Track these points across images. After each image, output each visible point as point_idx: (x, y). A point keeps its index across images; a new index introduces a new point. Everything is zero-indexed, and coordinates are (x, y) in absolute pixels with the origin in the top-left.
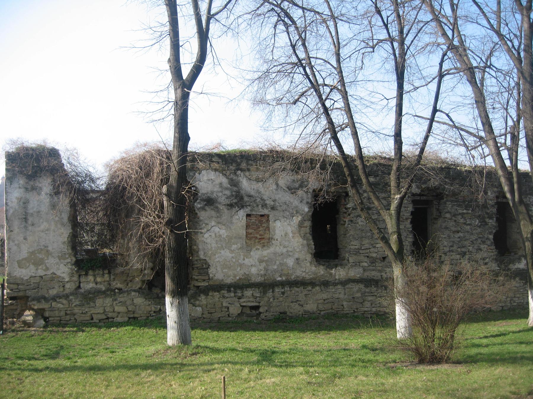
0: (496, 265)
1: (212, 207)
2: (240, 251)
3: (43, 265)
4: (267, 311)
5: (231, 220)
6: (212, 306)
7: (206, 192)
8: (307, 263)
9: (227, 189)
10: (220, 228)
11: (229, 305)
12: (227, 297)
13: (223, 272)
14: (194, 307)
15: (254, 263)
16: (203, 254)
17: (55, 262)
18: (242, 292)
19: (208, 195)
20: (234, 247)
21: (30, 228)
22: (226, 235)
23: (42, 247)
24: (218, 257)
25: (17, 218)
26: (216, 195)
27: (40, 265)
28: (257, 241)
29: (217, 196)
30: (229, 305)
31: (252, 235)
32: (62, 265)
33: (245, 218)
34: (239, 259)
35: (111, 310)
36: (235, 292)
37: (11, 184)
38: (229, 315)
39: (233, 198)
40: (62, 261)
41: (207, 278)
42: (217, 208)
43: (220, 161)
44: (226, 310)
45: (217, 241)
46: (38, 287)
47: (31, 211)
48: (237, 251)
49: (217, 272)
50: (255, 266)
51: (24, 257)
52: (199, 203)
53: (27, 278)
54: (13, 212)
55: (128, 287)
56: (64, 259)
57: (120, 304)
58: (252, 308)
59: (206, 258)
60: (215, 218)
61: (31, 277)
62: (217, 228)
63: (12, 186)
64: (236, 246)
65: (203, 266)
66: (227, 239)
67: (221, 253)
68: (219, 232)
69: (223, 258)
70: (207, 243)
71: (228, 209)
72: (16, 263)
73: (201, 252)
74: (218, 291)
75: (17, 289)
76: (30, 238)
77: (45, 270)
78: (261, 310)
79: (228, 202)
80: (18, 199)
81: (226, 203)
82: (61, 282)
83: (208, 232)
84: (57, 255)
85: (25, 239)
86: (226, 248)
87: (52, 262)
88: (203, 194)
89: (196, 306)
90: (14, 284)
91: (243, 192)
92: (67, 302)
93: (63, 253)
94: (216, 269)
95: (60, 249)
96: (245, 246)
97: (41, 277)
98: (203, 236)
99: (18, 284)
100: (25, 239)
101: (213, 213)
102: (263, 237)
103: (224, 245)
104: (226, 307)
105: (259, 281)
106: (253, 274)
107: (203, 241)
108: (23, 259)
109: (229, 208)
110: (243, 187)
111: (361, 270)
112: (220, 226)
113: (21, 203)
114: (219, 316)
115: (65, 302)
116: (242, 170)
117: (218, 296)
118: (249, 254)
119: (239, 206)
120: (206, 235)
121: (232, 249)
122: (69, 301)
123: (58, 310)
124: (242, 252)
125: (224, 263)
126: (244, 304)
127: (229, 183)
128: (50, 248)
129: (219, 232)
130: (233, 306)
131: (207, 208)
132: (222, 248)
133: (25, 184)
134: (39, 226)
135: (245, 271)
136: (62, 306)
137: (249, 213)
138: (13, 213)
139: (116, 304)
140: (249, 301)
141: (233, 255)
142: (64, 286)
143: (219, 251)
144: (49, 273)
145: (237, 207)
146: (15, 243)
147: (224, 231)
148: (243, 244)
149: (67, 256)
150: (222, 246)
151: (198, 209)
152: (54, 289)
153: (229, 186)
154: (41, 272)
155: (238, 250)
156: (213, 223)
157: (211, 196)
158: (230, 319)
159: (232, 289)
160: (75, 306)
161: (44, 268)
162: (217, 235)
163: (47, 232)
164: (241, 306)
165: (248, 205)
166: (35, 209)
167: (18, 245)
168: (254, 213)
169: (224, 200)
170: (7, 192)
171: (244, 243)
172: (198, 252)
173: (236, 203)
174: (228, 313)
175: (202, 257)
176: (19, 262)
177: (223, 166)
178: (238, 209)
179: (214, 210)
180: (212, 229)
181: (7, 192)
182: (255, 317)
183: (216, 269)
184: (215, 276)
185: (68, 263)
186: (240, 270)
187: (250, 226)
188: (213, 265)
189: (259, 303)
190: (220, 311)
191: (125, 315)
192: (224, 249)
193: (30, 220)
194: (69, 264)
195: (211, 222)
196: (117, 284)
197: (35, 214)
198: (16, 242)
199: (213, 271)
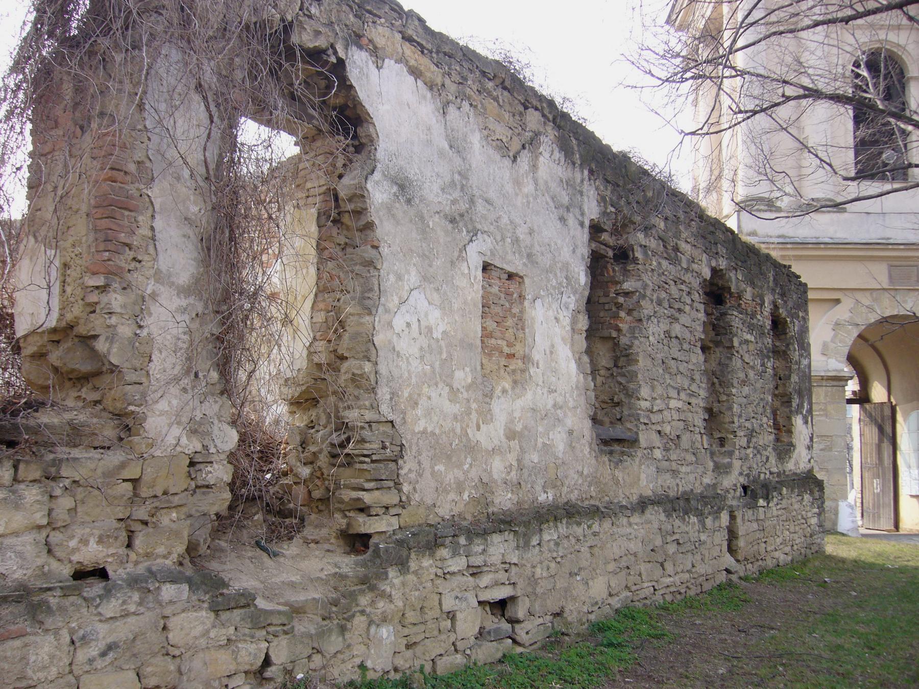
0: (496, 442)
8: (268, 492)
16: (388, 397)
22: (441, 328)
41: (396, 500)
48: (465, 395)
55: (133, 556)
66: (442, 343)
139: (91, 661)
172: (373, 390)
196: (84, 542)
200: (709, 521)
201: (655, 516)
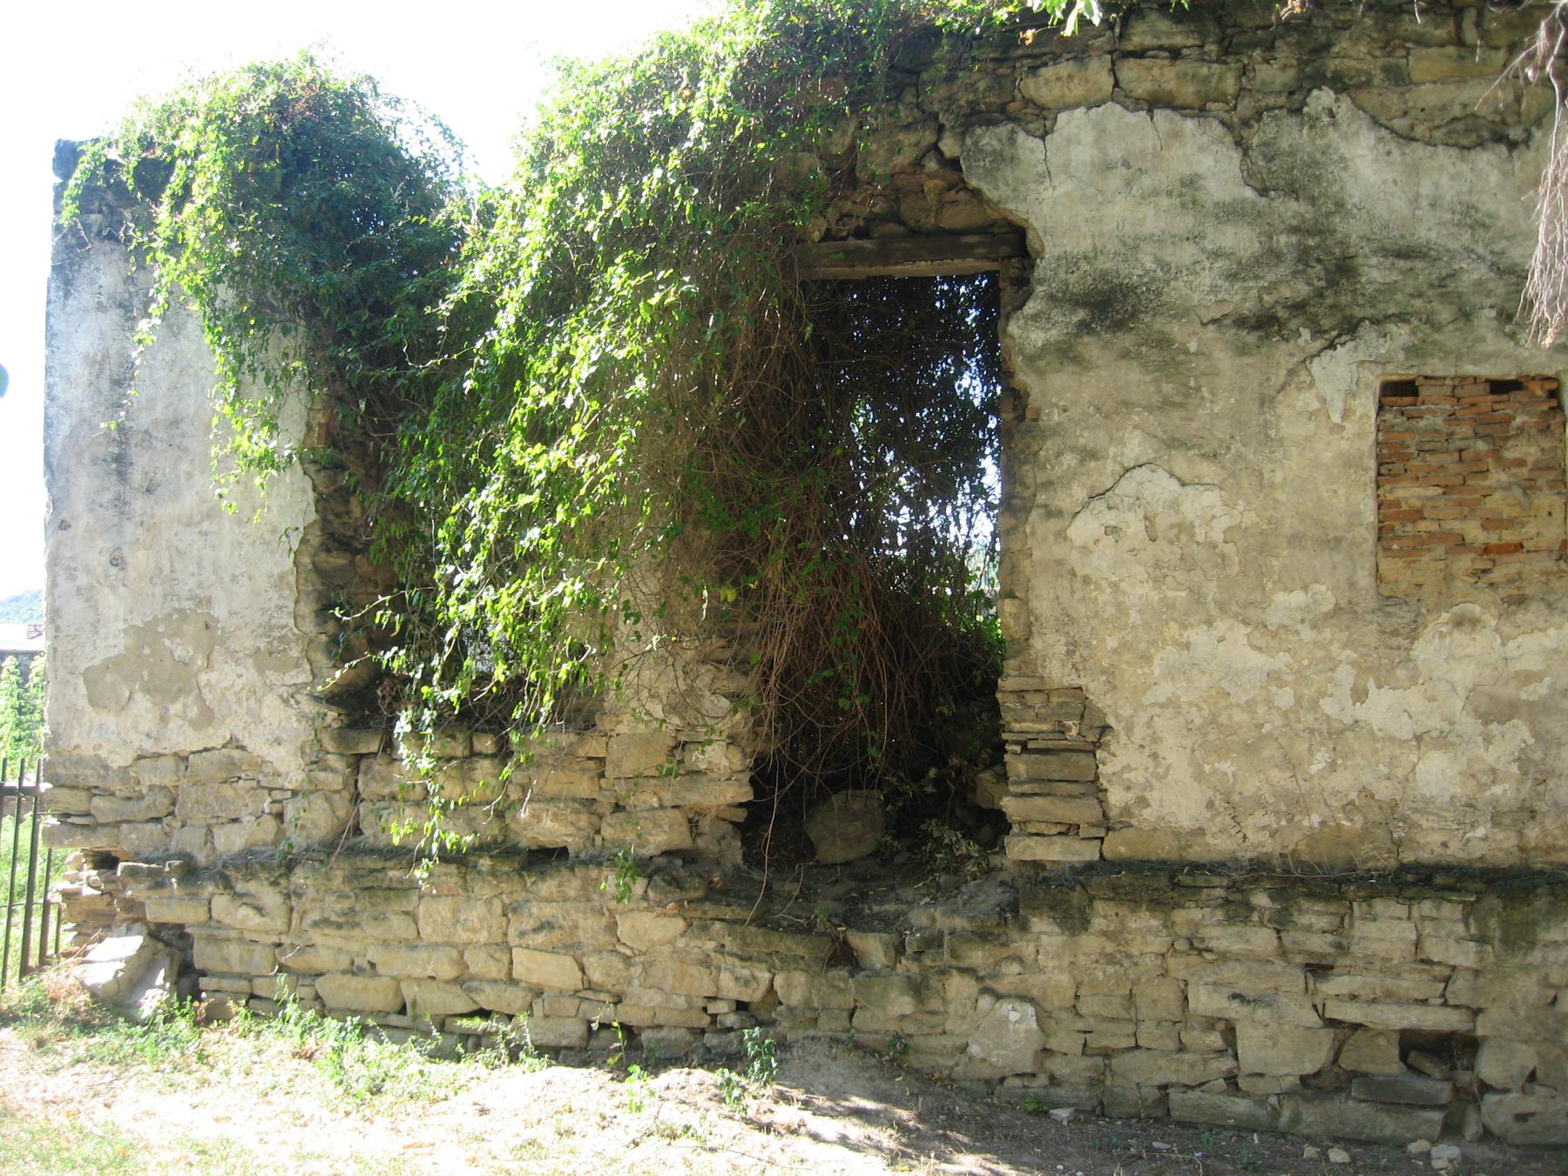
1: (1126, 340)
2: (1327, 634)
3: (191, 699)
4: (1532, 1077)
5: (1266, 425)
6: (1116, 1008)
7: (1085, 245)
9: (1231, 213)
10: (1187, 477)
11: (1235, 1010)
12: (1224, 957)
13: (1199, 776)
14: (985, 1002)
15: (1435, 723)
16: (1061, 649)
17: (240, 682)
18: (1338, 929)
19: (1104, 264)
20: (1287, 602)
21: (139, 505)
22: (1221, 524)
23: (187, 604)
24: (1171, 673)
25: (87, 457)
26: (1158, 261)
27: (175, 699)
28: (1465, 562)
29: (1164, 266)
30: (1235, 1010)
31: (1423, 526)
32: (271, 701)
33: (1366, 404)
34: (1323, 694)
35: (496, 970)
36: (1281, 923)
37: (67, 295)
38: (1231, 1080)
39: (1283, 270)
40: (272, 676)
42: (1163, 342)
43: (1178, 40)
44: (1215, 1039)
45: (1157, 565)
46: (169, 811)
47: (143, 421)
48: (1307, 634)
49: (1160, 778)
50: (1443, 741)
51: (113, 653)
52: (1035, 317)
53: (123, 763)
54: (74, 428)
56: (282, 669)
57: (540, 938)
58: (1413, 1044)
59: (1082, 682)
60: (1149, 408)
61: (140, 757)
62: (1161, 475)
63: (71, 301)
64: (1298, 598)
65: (1062, 731)
66: (1230, 549)
67: (1187, 646)
68: (1174, 505)
69: (1203, 682)
70: (1086, 580)
71: (1242, 350)
72: (80, 681)
73: (1051, 638)
74: (1158, 904)
75: (87, 814)
76: (138, 559)
77: (197, 725)
78: (1489, 1067)
79: (1242, 298)
80: (94, 362)
81: (1227, 309)
82: (271, 790)
83: (1099, 505)
84: (249, 644)
85: (117, 562)
86: (1222, 608)
87: (227, 684)
88: (1071, 262)
89: (999, 997)
90: (73, 787)
91: (1351, 230)
92: (279, 899)
93: (276, 634)
94: (1155, 756)
95: (264, 611)
96: (1369, 601)
97: (182, 758)
98: (1061, 535)
99: (92, 791)
100: (117, 562)
101: (1133, 378)
102: (1509, 536)
103: (1211, 590)
104: (1210, 1023)
105: (1477, 850)
106: (1428, 801)
107: (1060, 562)
108: (106, 667)
109: (1251, 338)
110: (1354, 195)
112: (1181, 465)
113: (105, 385)
114: (1159, 1079)
115: (271, 898)
116: (1340, 84)
117: (1157, 944)
118: (1397, 656)
119: (1326, 323)
120: (1083, 529)
121: (1273, 619)
122: (288, 896)
123: (241, 940)
124: (1345, 646)
125: (1213, 720)
126: (1351, 1013)
127: (1249, 177)
128: (219, 611)
129: (1174, 505)
130: (1262, 1014)
131: (1090, 347)
132: (1197, 609)
133: (121, 288)
134: (176, 495)
135: (1367, 778)
136: (254, 920)
137: (1398, 372)
138: (70, 436)
140: (1390, 996)
141: (1281, 660)
142: (280, 816)
143: (1173, 630)
144: (219, 742)
145: (1306, 334)
146: (78, 583)
147: (1211, 498)
148: (1352, 585)
149: (295, 652)
150: (1197, 597)
151: (1031, 359)
152: (236, 825)
153: (1249, 193)
154: (184, 739)
155: (1314, 626)
156: (1134, 446)
157: (1124, 269)
158: (1241, 1106)
159: (1261, 899)
160: (316, 924)
161: (194, 712)
162: (1162, 522)
163: (205, 526)
164: (1331, 1023)
165: (1387, 317)
166: (159, 411)
167: (87, 594)
168: (1434, 366)
169: (1214, 289)
170: (54, 335)
171: (1364, 579)
173: (1298, 307)
174: (1226, 1064)
175: (1057, 673)
176: (90, 677)
177: (1204, 70)
178: (1318, 344)
179: (1139, 355)
180: (1128, 486)
181: (54, 335)
182: (1437, 1116)
183: (1155, 756)
184: (1143, 802)
185: (298, 688)
186: (1332, 766)
187: (1406, 458)
188: (1129, 730)
189: (1476, 1012)
190: (1171, 1045)
191: (570, 1005)
192: (1209, 623)
193: (141, 462)
194: (303, 699)
195: (1121, 442)
197: (161, 435)
198: (83, 580)
199: (1128, 768)
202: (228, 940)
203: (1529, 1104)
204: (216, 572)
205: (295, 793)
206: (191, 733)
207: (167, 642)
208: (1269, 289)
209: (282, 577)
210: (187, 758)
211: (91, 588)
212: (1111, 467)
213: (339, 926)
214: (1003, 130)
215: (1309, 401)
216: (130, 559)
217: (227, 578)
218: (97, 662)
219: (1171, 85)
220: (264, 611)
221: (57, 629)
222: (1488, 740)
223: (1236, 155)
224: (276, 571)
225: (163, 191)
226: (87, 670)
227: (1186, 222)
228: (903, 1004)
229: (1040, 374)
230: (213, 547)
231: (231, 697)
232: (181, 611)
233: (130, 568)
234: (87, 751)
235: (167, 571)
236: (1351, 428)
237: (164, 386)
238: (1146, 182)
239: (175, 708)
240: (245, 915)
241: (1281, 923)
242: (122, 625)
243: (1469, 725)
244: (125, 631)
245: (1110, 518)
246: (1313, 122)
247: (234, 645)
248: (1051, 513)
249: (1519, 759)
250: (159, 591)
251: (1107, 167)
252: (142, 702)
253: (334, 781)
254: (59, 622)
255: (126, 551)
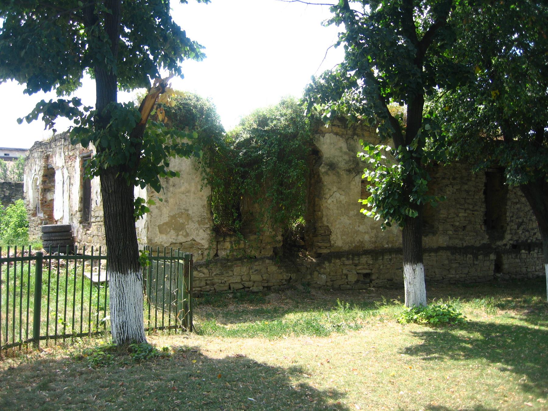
1: (334, 172)
14: (320, 275)
17: (194, 227)
19: (331, 159)
21: (171, 189)
22: (345, 201)
27: (180, 231)
29: (338, 160)
30: (348, 273)
32: (201, 231)
33: (360, 184)
36: (353, 259)
39: (351, 163)
40: (202, 226)
42: (338, 173)
43: (339, 124)
48: (354, 218)
50: (368, 233)
52: (323, 167)
61: (171, 244)
65: (325, 232)
70: (329, 209)
77: (185, 236)
78: (373, 277)
83: (331, 198)
84: (197, 219)
88: (327, 158)
89: (321, 274)
95: (200, 212)
97: (181, 244)
98: (327, 202)
108: (164, 224)
111: (447, 238)
115: (206, 271)
117: (339, 263)
120: (329, 201)
125: (343, 230)
127: (348, 148)
128: (190, 212)
129: (339, 198)
131: (330, 172)
134: (180, 187)
140: (364, 269)
142: (202, 254)
143: (339, 217)
147: (343, 197)
149: (206, 221)
151: (322, 174)
153: (347, 150)
154: (181, 239)
161: (185, 234)
163: (187, 194)
164: (358, 273)
173: (353, 169)
174: (347, 281)
175: (325, 223)
176: (159, 227)
184: (335, 243)
192: (343, 216)
200: (480, 257)
201: (444, 255)
202: (196, 280)
203: (377, 282)
204: (189, 204)
205: (206, 249)
206: (184, 238)
207: (178, 219)
208: (350, 166)
209: (204, 206)
210: (181, 244)
211: (160, 207)
212: (332, 192)
213: (220, 275)
214: (318, 135)
215: (354, 183)
216: (169, 201)
217: (192, 206)
218: (161, 223)
219: (338, 132)
220: (200, 212)
221: (151, 216)
222: (372, 232)
223: (346, 144)
224: (203, 204)
225: (117, 88)
226: (159, 225)
227: (340, 154)
228: (309, 277)
229: (324, 176)
230: (189, 199)
231: (192, 230)
232: (182, 212)
233: (169, 203)
234: (159, 243)
235: (178, 203)
236: (358, 188)
237: (177, 163)
238: (336, 147)
239: (181, 233)
240: (201, 275)
241: (353, 259)
242: (167, 215)
243: (370, 230)
244: (168, 217)
245: (332, 200)
246: (354, 140)
247: (193, 219)
248: (326, 199)
249: (529, 301)
250: (176, 207)
251: (331, 144)
252: (172, 232)
253: (215, 246)
254: (152, 214)
255: (168, 199)
